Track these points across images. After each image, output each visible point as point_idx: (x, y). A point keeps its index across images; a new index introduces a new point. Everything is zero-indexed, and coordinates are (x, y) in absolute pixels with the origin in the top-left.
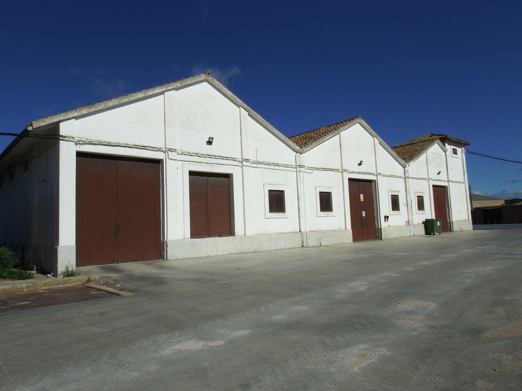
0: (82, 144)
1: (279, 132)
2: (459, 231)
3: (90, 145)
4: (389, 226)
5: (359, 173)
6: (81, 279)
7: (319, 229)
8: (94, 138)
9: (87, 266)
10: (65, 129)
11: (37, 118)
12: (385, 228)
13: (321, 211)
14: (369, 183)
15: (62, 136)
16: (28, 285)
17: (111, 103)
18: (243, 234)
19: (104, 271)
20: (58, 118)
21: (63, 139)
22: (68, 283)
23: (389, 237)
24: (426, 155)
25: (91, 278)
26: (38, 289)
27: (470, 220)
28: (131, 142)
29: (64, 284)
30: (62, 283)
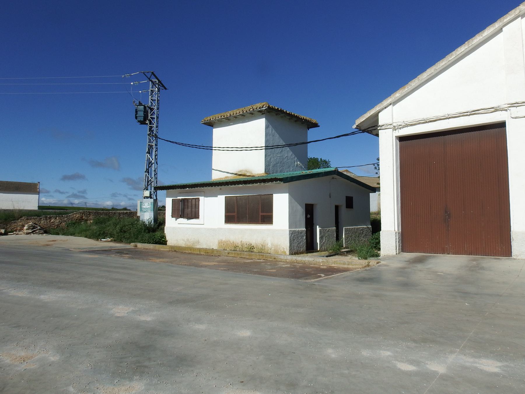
0: (400, 128)
1: (445, 59)
3: (408, 127)
6: (361, 263)
8: (410, 119)
9: (465, 255)
10: (383, 119)
11: (358, 117)
15: (380, 126)
16: (323, 261)
17: (424, 76)
20: (374, 110)
21: (381, 128)
22: (351, 265)
25: (370, 263)
26: (330, 265)
28: (440, 114)
29: (348, 264)
30: (320, 261)
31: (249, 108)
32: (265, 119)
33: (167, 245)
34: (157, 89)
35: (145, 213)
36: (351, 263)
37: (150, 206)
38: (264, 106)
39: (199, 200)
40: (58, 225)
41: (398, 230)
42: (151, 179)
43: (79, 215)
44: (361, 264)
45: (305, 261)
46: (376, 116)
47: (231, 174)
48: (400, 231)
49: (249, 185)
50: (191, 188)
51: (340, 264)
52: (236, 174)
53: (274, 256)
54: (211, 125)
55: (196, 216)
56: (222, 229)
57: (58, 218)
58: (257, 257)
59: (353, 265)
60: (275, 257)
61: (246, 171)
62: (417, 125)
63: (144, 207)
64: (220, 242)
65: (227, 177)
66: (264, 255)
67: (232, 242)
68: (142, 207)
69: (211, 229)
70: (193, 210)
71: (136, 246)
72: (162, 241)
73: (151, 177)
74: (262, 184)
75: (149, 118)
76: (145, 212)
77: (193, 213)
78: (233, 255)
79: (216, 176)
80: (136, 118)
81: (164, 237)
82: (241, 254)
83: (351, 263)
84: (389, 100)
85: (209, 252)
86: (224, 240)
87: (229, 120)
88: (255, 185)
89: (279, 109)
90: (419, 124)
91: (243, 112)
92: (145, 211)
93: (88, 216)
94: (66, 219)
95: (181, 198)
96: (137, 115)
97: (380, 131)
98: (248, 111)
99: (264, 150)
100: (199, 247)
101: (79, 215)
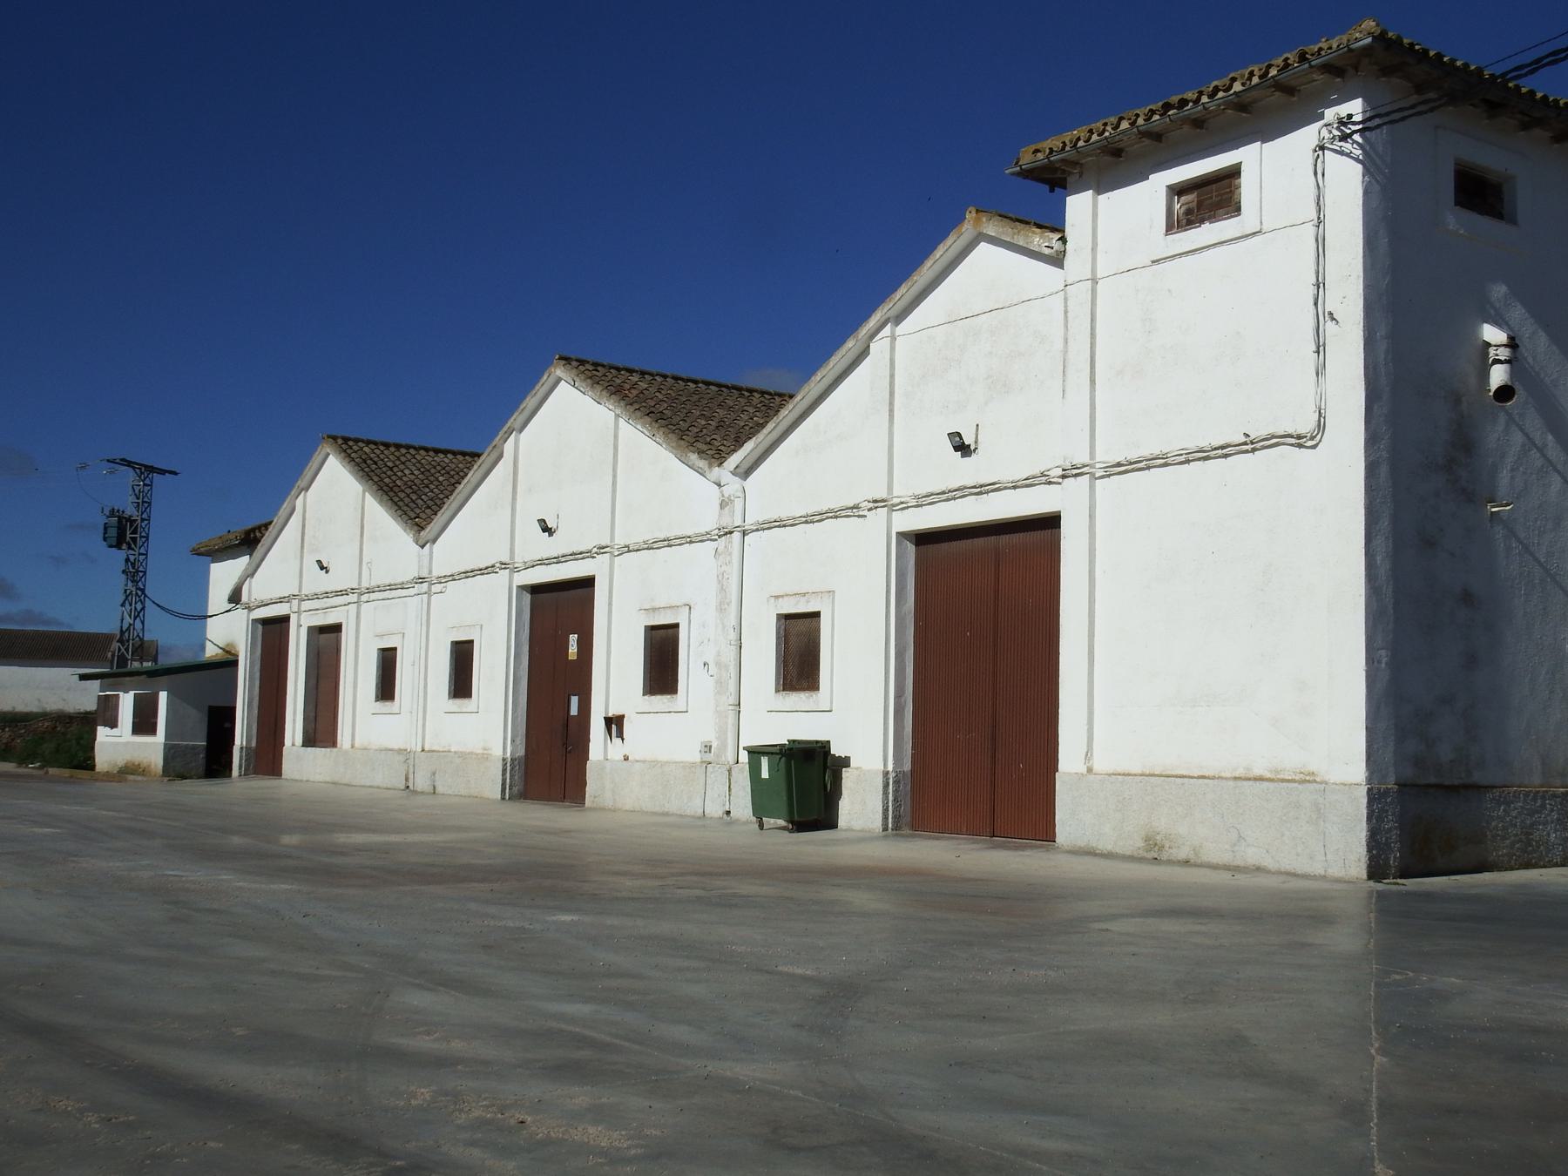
2: (427, 791)
4: (626, 759)
5: (558, 560)
7: (444, 747)
12: (102, 743)
13: (210, 706)
14: (333, 635)
18: (602, 758)
19: (985, 846)
23: (609, 803)
24: (1536, 65)
27: (297, 744)
33: (93, 767)
40: (6, 744)
41: (248, 741)
43: (49, 723)
48: (907, 767)
57: (7, 729)
67: (137, 763)
75: (128, 539)
80: (105, 539)
89: (1539, 95)
93: (68, 725)
94: (23, 731)
101: (49, 723)
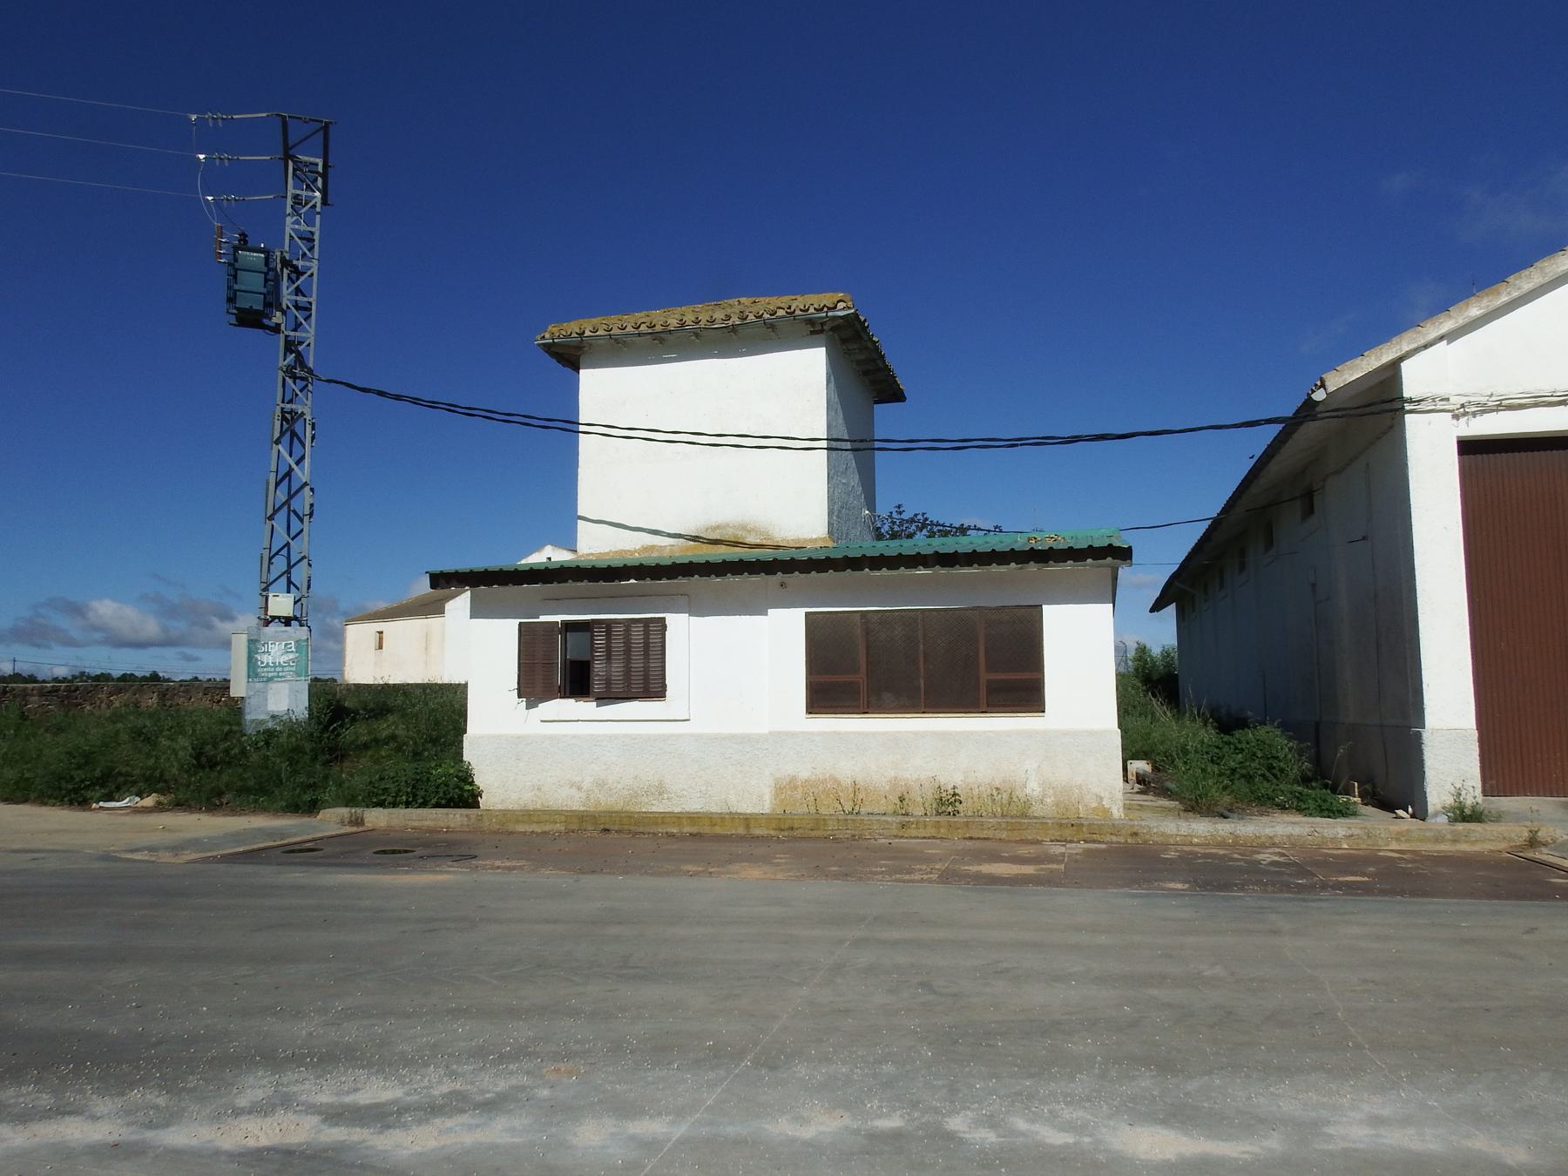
0: (1474, 414)
8: (1512, 388)
10: (1416, 379)
15: (1411, 401)
16: (1350, 832)
22: (1466, 842)
25: (1539, 834)
26: (1380, 846)
29: (1455, 841)
30: (1340, 836)
31: (768, 304)
32: (824, 348)
34: (317, 194)
35: (273, 686)
36: (1466, 836)
37: (291, 656)
38: (841, 305)
39: (664, 627)
42: (290, 541)
44: (1504, 838)
45: (1275, 836)
46: (1394, 367)
47: (670, 535)
49: (966, 570)
50: (652, 579)
51: (1421, 841)
52: (695, 539)
53: (1133, 826)
54: (571, 357)
55: (651, 686)
56: (793, 735)
58: (1051, 832)
59: (1474, 843)
60: (1135, 830)
61: (743, 527)
62: (1529, 407)
63: (266, 659)
64: (784, 788)
65: (652, 548)
66: (1082, 825)
68: (257, 659)
69: (732, 737)
70: (637, 664)
71: (358, 822)
72: (463, 794)
73: (289, 535)
74: (1032, 567)
76: (270, 680)
77: (637, 679)
78: (931, 831)
79: (594, 544)
81: (466, 777)
82: (967, 826)
83: (1466, 836)
84: (1447, 324)
85: (796, 825)
86: (804, 774)
87: (662, 341)
88: (995, 569)
90: (1536, 405)
91: (746, 319)
92: (270, 675)
95: (559, 618)
96: (236, 287)
97: (1407, 416)
98: (766, 316)
99: (826, 451)
100: (670, 810)
